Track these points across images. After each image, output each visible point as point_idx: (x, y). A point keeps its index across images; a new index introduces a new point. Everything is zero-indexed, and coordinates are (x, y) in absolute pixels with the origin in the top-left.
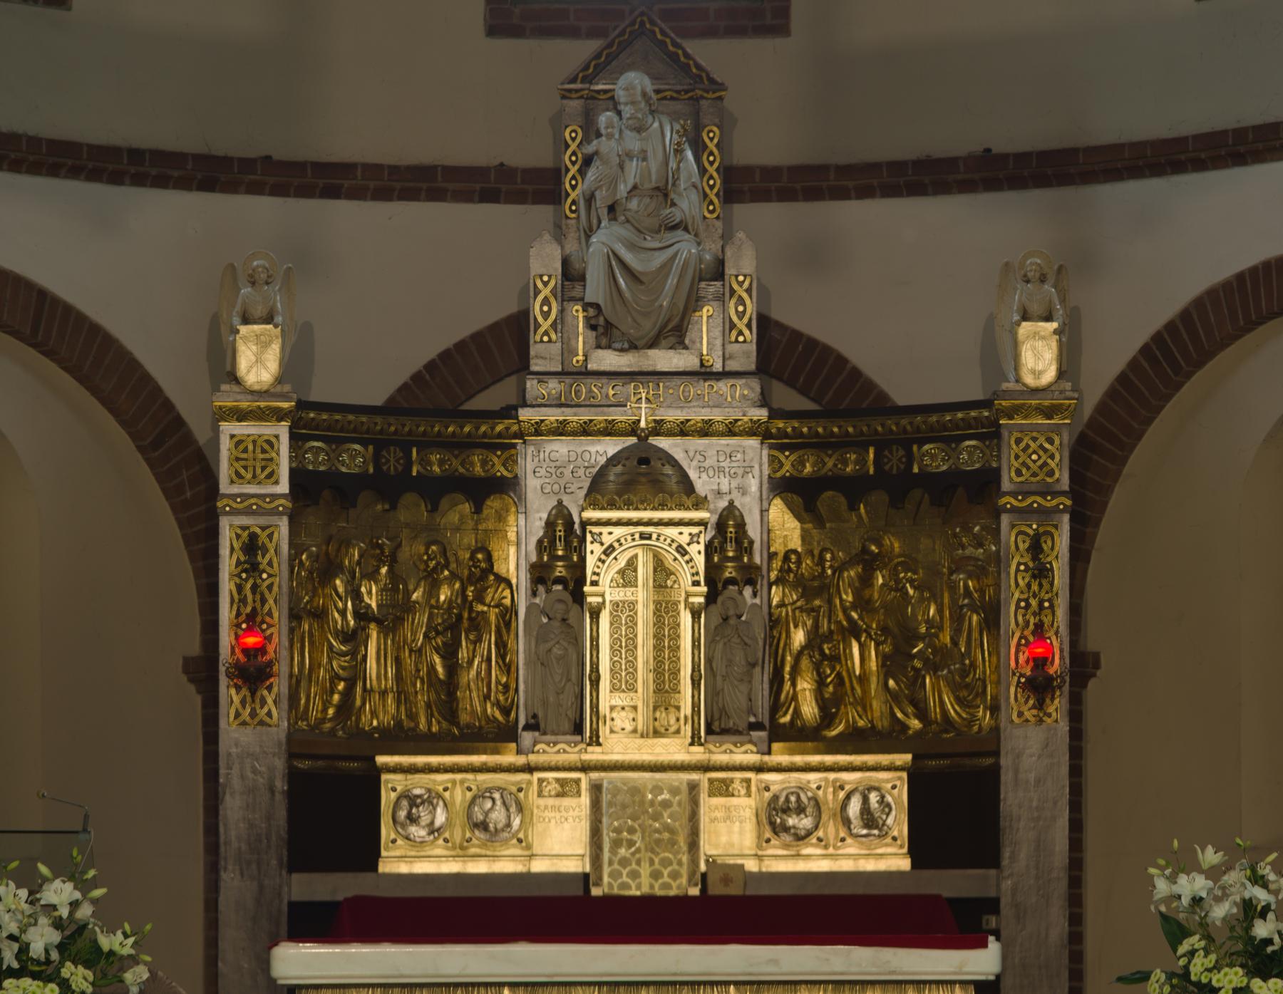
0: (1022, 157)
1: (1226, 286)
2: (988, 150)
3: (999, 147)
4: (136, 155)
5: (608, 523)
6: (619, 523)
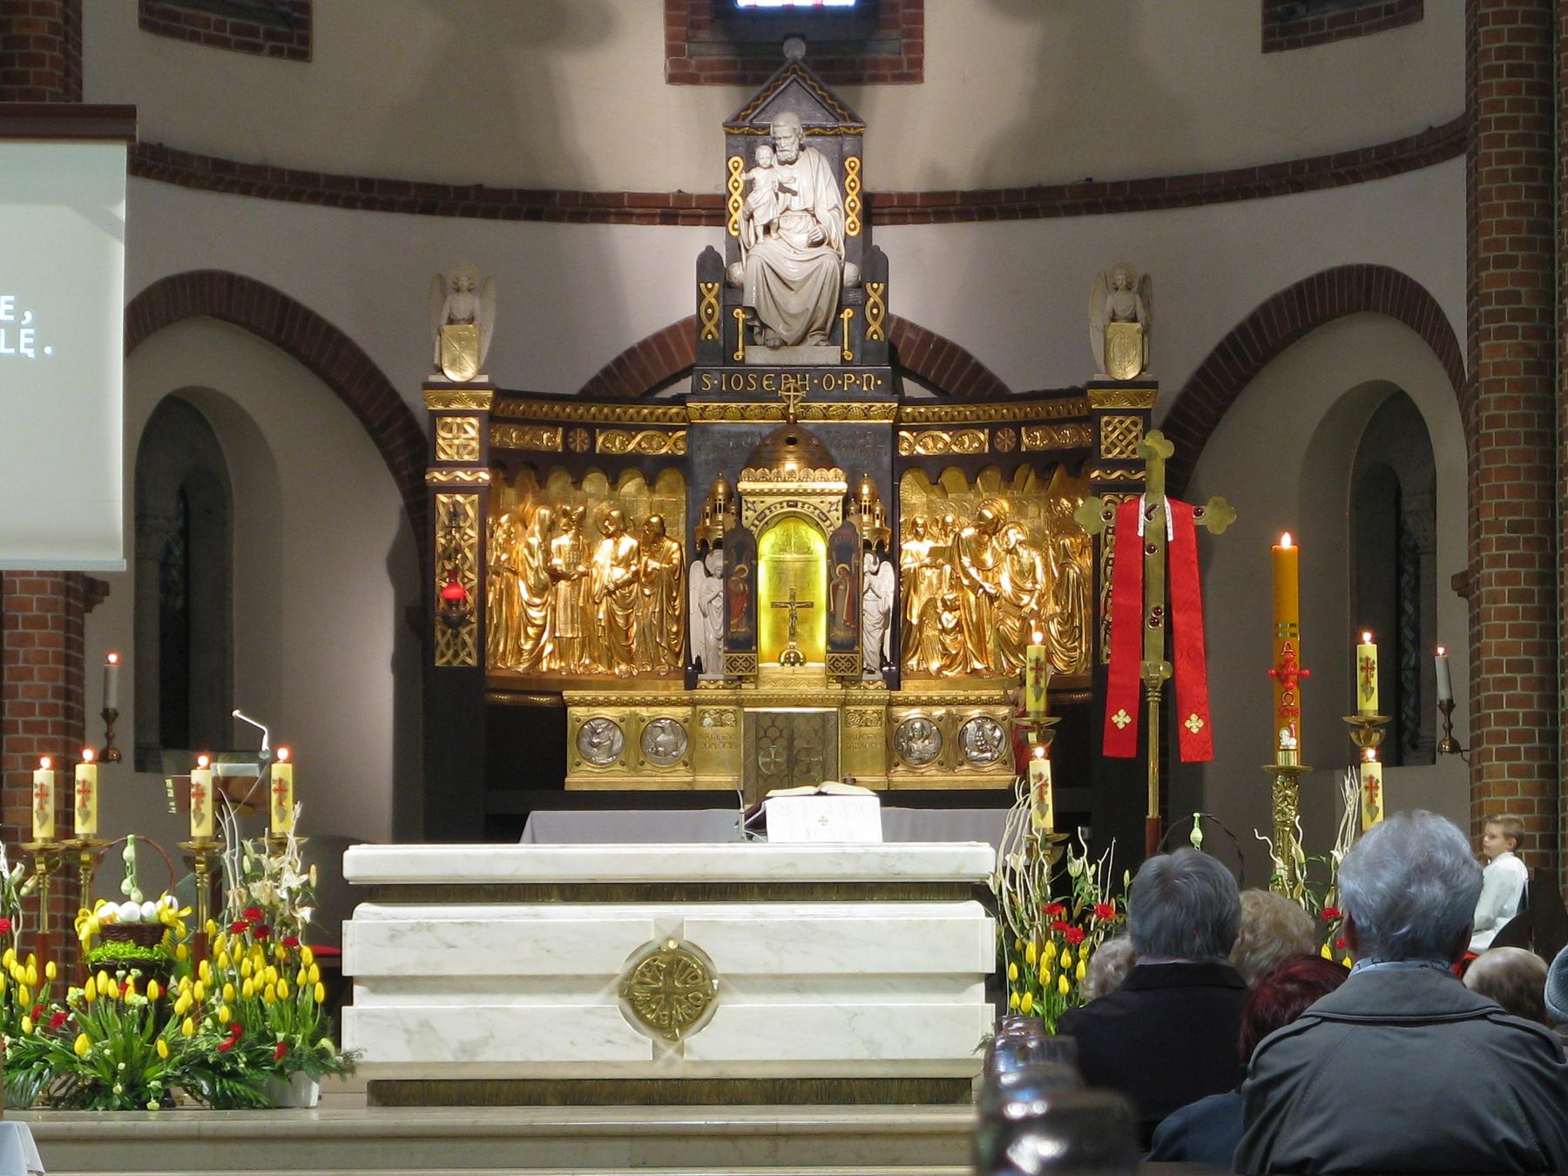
0: (1118, 186)
1: (1287, 294)
2: (1090, 180)
3: (1098, 178)
4: (367, 183)
5: (762, 493)
6: (770, 493)
